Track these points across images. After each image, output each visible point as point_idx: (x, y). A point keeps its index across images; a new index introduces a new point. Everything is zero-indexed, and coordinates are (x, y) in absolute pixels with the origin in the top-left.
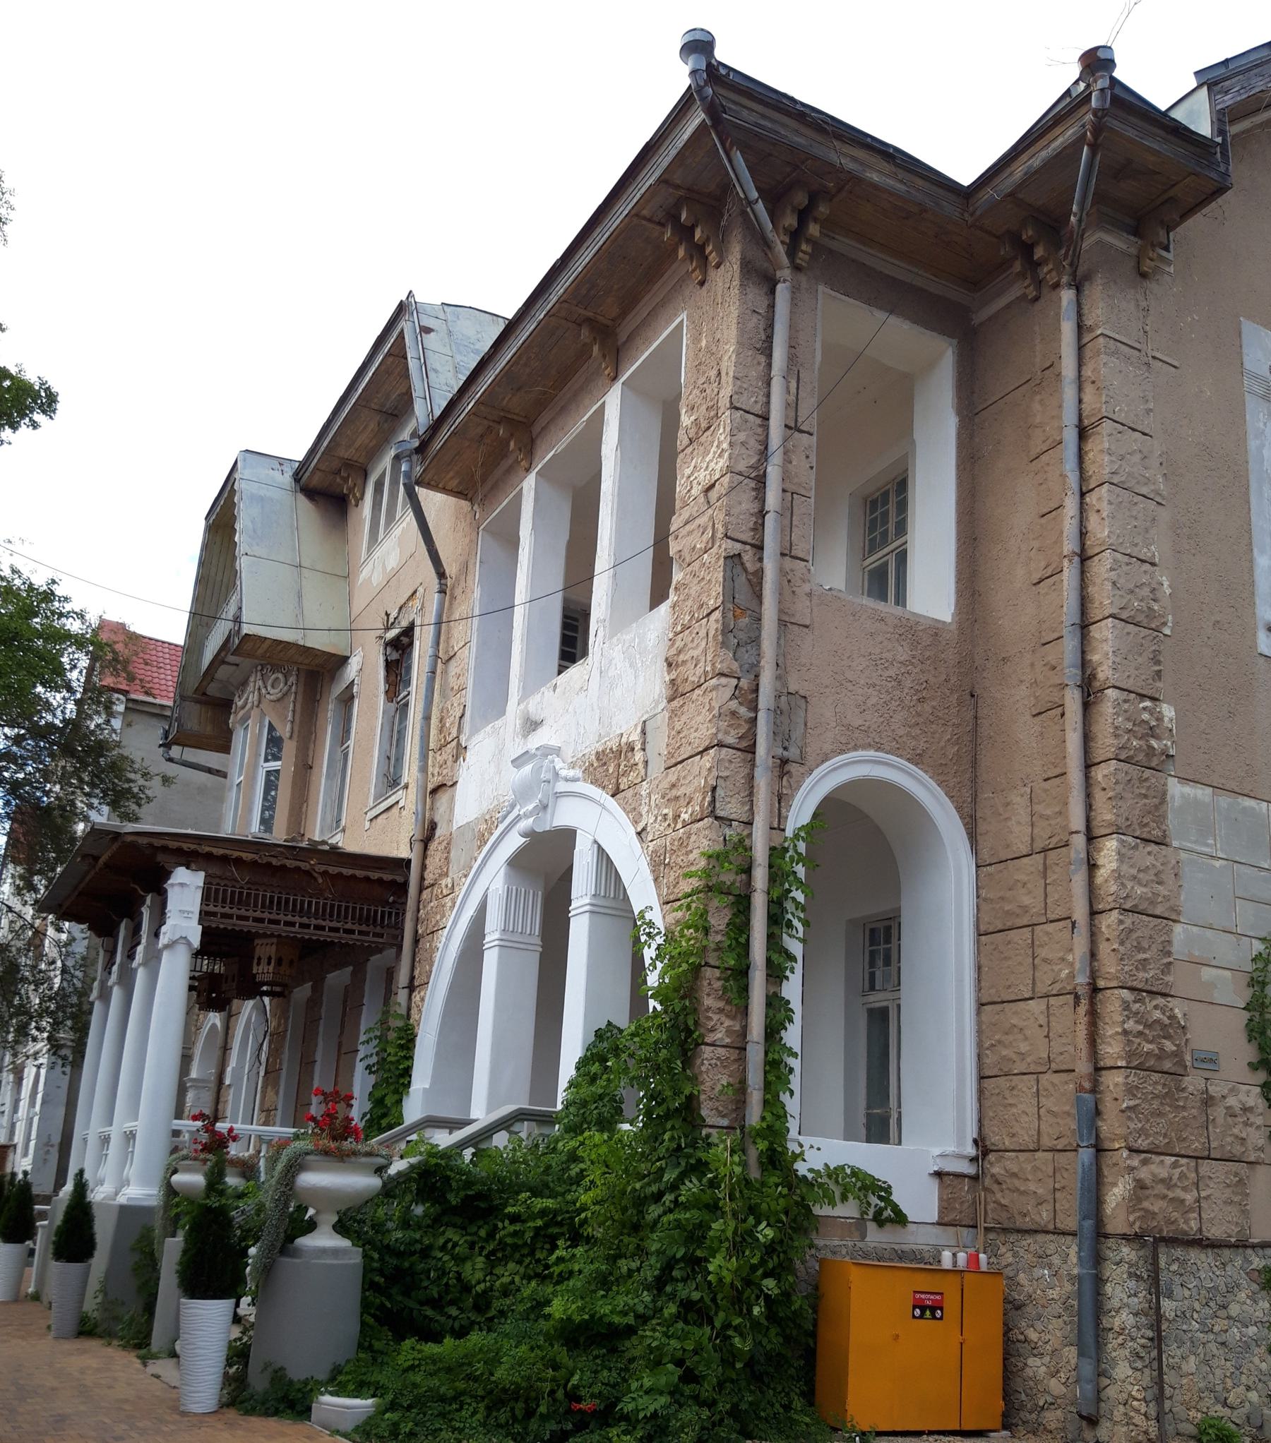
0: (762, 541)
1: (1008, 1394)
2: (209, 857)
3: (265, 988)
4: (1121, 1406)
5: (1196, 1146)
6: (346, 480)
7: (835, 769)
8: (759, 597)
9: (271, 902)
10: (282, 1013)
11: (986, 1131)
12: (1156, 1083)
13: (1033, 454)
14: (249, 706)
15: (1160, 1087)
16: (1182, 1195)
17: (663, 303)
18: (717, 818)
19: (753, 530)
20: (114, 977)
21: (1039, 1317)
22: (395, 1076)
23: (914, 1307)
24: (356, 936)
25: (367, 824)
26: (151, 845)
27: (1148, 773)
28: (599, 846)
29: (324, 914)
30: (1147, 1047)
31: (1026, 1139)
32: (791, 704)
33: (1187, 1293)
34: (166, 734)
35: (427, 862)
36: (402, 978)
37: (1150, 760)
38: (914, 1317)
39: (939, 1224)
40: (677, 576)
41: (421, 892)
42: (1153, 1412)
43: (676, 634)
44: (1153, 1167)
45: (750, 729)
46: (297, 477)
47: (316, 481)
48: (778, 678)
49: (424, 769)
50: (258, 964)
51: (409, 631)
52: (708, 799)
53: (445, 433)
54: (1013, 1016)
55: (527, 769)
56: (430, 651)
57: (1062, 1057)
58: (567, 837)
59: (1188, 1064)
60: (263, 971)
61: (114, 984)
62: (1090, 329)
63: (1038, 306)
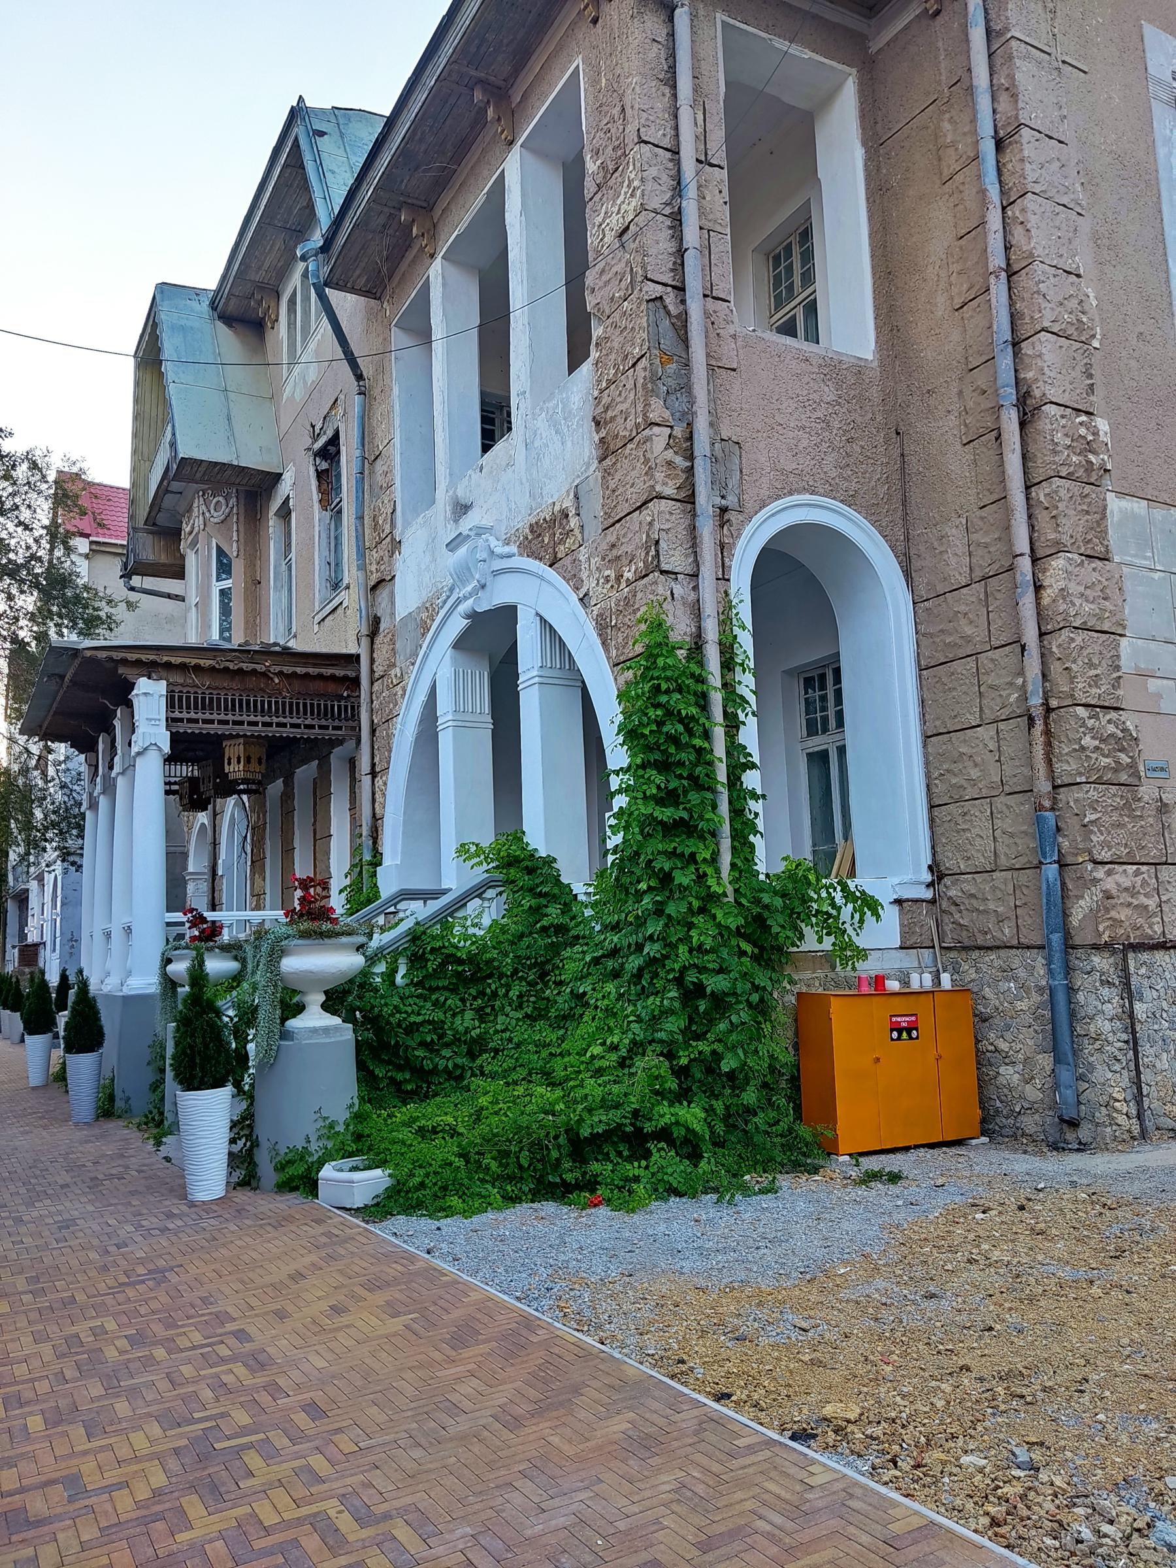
0: (683, 282)
1: (983, 1102)
2: (168, 666)
3: (242, 787)
4: (1103, 1108)
5: (1154, 854)
6: (260, 303)
7: (773, 515)
8: (685, 341)
9: (233, 705)
10: (259, 807)
11: (939, 857)
12: (1114, 795)
13: (946, 173)
14: (196, 530)
15: (1118, 800)
16: (1146, 901)
17: (560, 47)
18: (662, 572)
19: (672, 270)
20: (98, 788)
21: (1008, 1027)
22: (368, 862)
23: (892, 1030)
24: (317, 731)
25: (316, 627)
26: (111, 659)
27: (1088, 489)
28: (541, 618)
29: (284, 712)
30: (1105, 761)
31: (981, 861)
32: (728, 449)
33: (1155, 994)
34: (125, 565)
35: (375, 655)
36: (364, 765)
37: (1089, 476)
38: (892, 1039)
39: (901, 948)
40: (597, 332)
41: (372, 684)
42: (1134, 1112)
43: (602, 391)
44: (1117, 877)
45: (687, 478)
46: (213, 306)
47: (231, 308)
48: (711, 424)
49: (362, 567)
50: (229, 764)
51: (335, 440)
52: (653, 552)
53: (347, 226)
54: (960, 745)
55: (462, 551)
56: (358, 453)
57: (1015, 780)
58: (509, 613)
59: (1142, 774)
60: (235, 770)
61: (99, 794)
62: (1000, 34)
63: (940, 19)
